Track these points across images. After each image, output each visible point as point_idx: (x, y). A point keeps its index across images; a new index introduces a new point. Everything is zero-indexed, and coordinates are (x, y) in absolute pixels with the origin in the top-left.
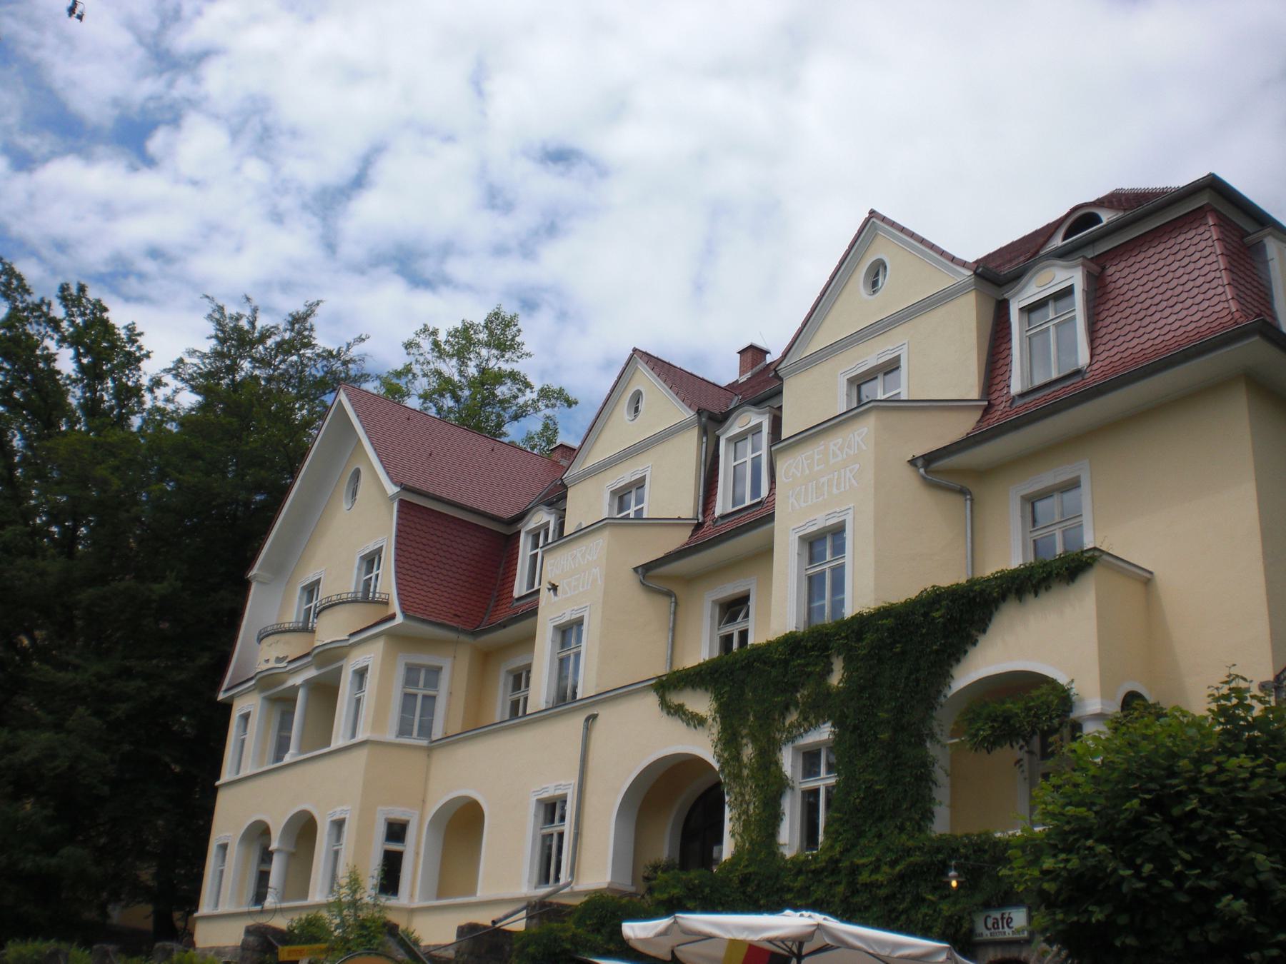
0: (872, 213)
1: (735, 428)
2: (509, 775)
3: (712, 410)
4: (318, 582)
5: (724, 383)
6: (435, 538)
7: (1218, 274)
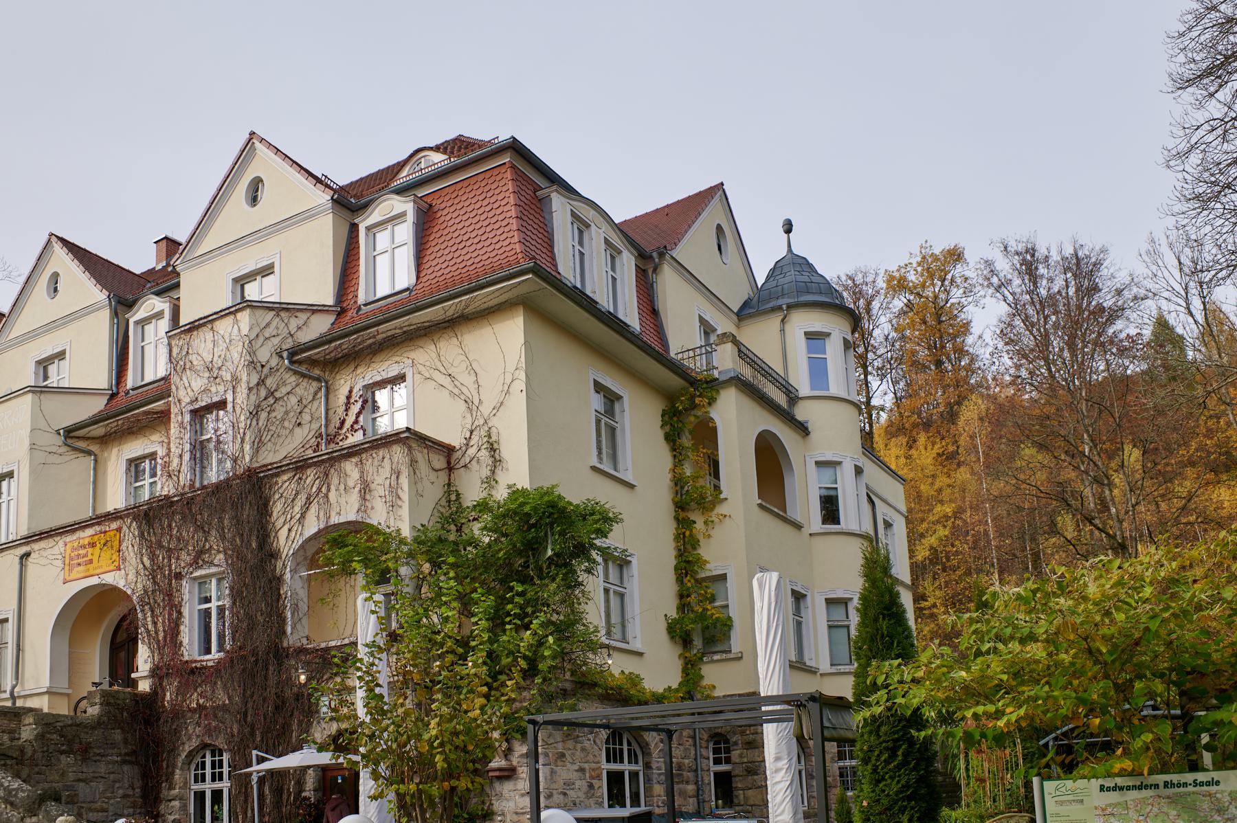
0: (252, 134)
3: (124, 290)
5: (138, 270)
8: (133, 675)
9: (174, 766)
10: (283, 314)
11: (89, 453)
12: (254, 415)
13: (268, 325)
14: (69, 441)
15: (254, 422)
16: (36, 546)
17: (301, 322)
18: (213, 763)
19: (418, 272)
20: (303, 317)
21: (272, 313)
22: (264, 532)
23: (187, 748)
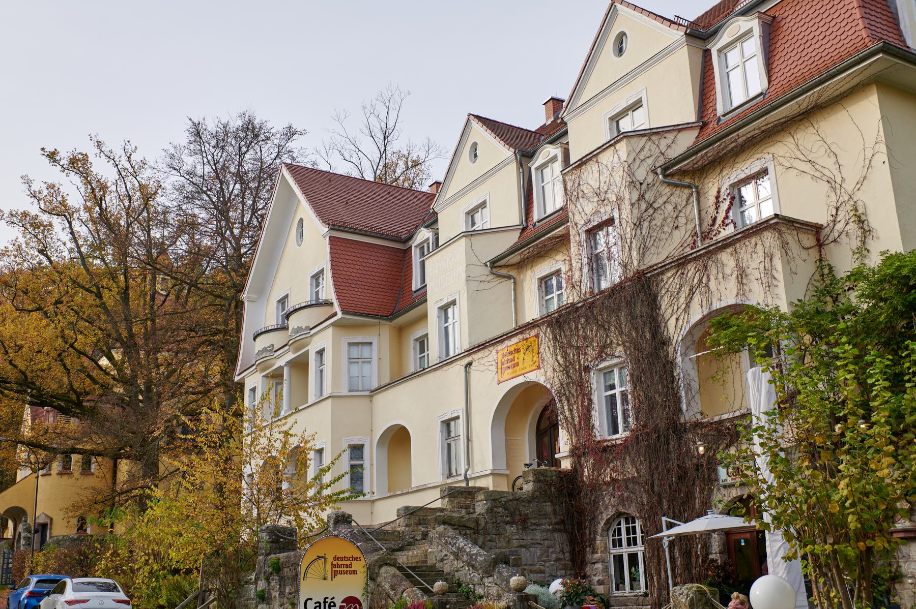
1: (540, 159)
2: (414, 406)
4: (287, 296)
6: (356, 259)
7: (853, 11)
9: (595, 533)
10: (654, 138)
12: (638, 225)
13: (642, 149)
14: (494, 270)
16: (475, 356)
18: (628, 530)
21: (645, 139)
22: (655, 323)
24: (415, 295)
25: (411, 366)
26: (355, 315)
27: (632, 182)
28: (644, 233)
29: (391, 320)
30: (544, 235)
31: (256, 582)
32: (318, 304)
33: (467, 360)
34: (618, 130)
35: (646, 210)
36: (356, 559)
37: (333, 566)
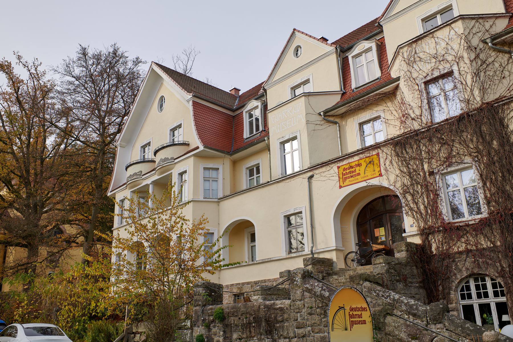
8: (404, 235)
9: (450, 289)
10: (481, 21)
11: (336, 123)
12: (477, 74)
13: (473, 27)
14: (326, 118)
15: (478, 78)
16: (317, 171)
17: (491, 23)
18: (477, 287)
19: (381, 70)
20: (491, 22)
21: (474, 21)
23: (459, 277)
24: (246, 141)
25: (244, 185)
26: (211, 149)
27: (470, 47)
28: (481, 79)
29: (231, 155)
30: (373, 92)
31: (191, 328)
32: (144, 161)
33: (309, 174)
34: (295, 95)
35: (481, 66)
36: (364, 309)
37: (351, 316)
